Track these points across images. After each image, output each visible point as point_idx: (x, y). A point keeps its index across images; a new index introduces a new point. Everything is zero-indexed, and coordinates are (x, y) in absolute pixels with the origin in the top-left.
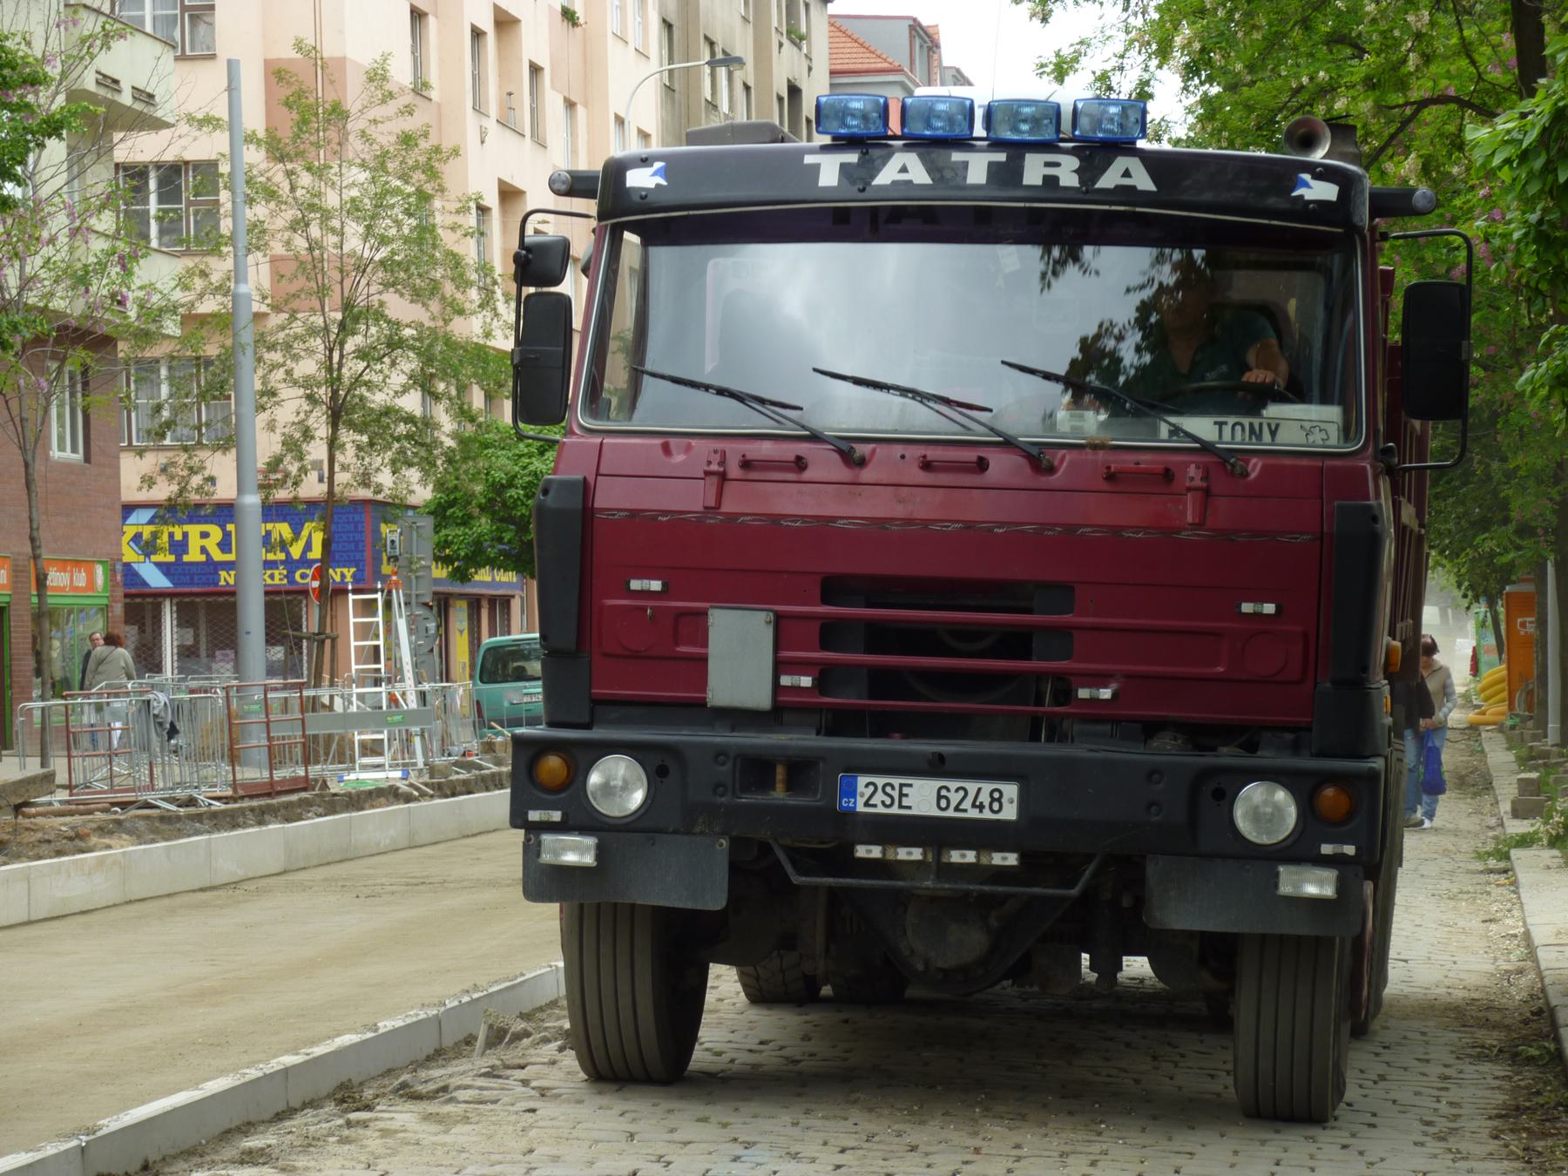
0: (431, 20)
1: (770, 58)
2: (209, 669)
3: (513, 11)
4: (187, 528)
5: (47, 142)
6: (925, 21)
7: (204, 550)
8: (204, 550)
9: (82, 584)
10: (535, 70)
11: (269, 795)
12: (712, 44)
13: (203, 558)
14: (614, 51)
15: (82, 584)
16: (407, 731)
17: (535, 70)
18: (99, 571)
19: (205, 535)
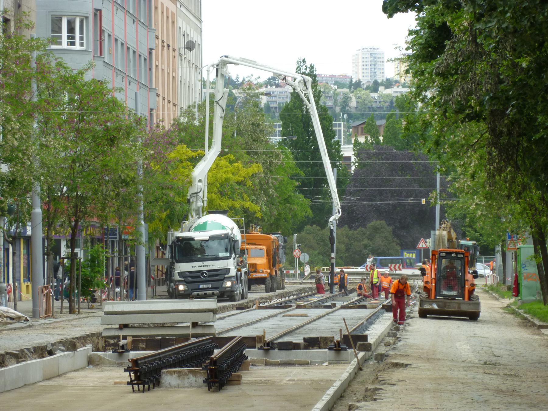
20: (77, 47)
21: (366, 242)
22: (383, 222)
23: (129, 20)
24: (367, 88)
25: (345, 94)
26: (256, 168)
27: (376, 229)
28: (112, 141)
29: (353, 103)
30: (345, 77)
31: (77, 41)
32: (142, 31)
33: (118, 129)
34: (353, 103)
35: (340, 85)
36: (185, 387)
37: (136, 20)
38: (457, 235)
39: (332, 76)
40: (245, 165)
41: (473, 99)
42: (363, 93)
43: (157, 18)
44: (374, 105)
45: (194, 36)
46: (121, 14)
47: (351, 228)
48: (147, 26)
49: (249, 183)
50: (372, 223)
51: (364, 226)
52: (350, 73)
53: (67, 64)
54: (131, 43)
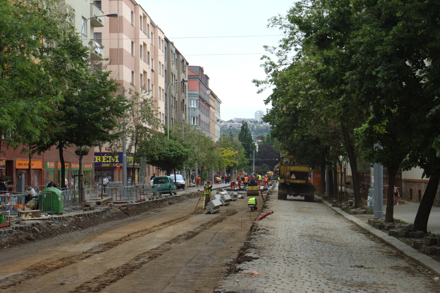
0: (134, 73)
1: (180, 75)
2: (98, 180)
3: (146, 71)
4: (109, 157)
5: (293, 62)
6: (201, 67)
7: (98, 160)
8: (98, 160)
9: (89, 167)
10: (149, 80)
11: (140, 202)
12: (172, 74)
13: (98, 162)
14: (159, 75)
15: (89, 167)
16: (232, 187)
17: (149, 80)
18: (92, 165)
19: (98, 158)
20: (195, 124)
21: (262, 170)
22: (266, 164)
23: (205, 116)
24: (259, 123)
25: (253, 125)
26: (237, 152)
27: (264, 166)
28: (212, 149)
29: (255, 127)
30: (252, 119)
31: (195, 123)
32: (208, 118)
33: (213, 147)
34: (255, 127)
35: (251, 122)
36: (127, 182)
37: (207, 116)
38: (300, 195)
39: (248, 119)
40: (234, 151)
41: (290, 92)
42: (258, 124)
43: (211, 114)
44: (261, 128)
45: (218, 118)
46: (204, 115)
47: (257, 166)
48: (209, 117)
49: (235, 156)
50: (263, 165)
51: (261, 165)
52: (254, 118)
53: (397, 268)
54: (206, 122)
